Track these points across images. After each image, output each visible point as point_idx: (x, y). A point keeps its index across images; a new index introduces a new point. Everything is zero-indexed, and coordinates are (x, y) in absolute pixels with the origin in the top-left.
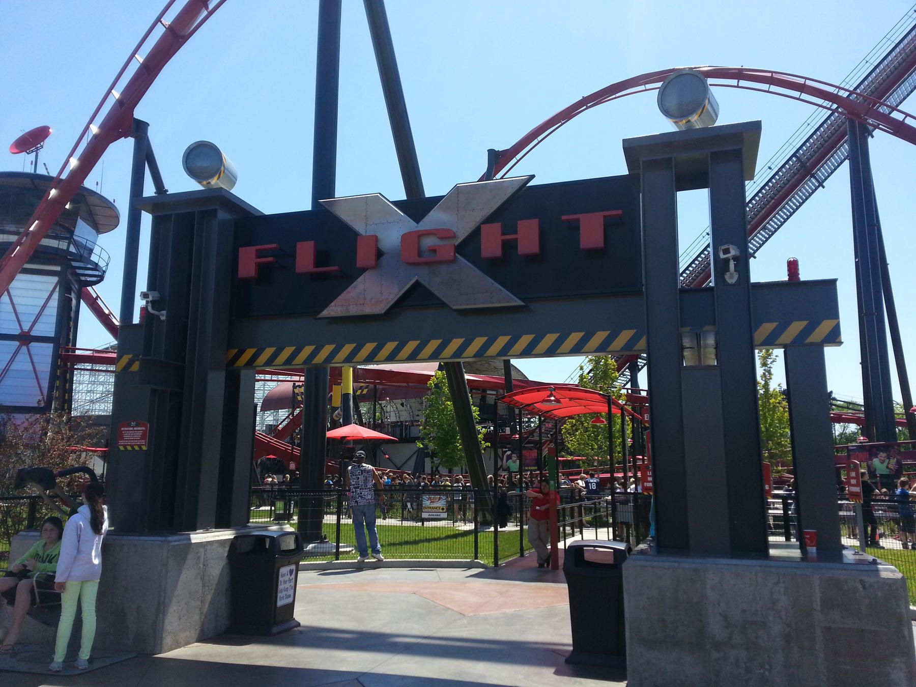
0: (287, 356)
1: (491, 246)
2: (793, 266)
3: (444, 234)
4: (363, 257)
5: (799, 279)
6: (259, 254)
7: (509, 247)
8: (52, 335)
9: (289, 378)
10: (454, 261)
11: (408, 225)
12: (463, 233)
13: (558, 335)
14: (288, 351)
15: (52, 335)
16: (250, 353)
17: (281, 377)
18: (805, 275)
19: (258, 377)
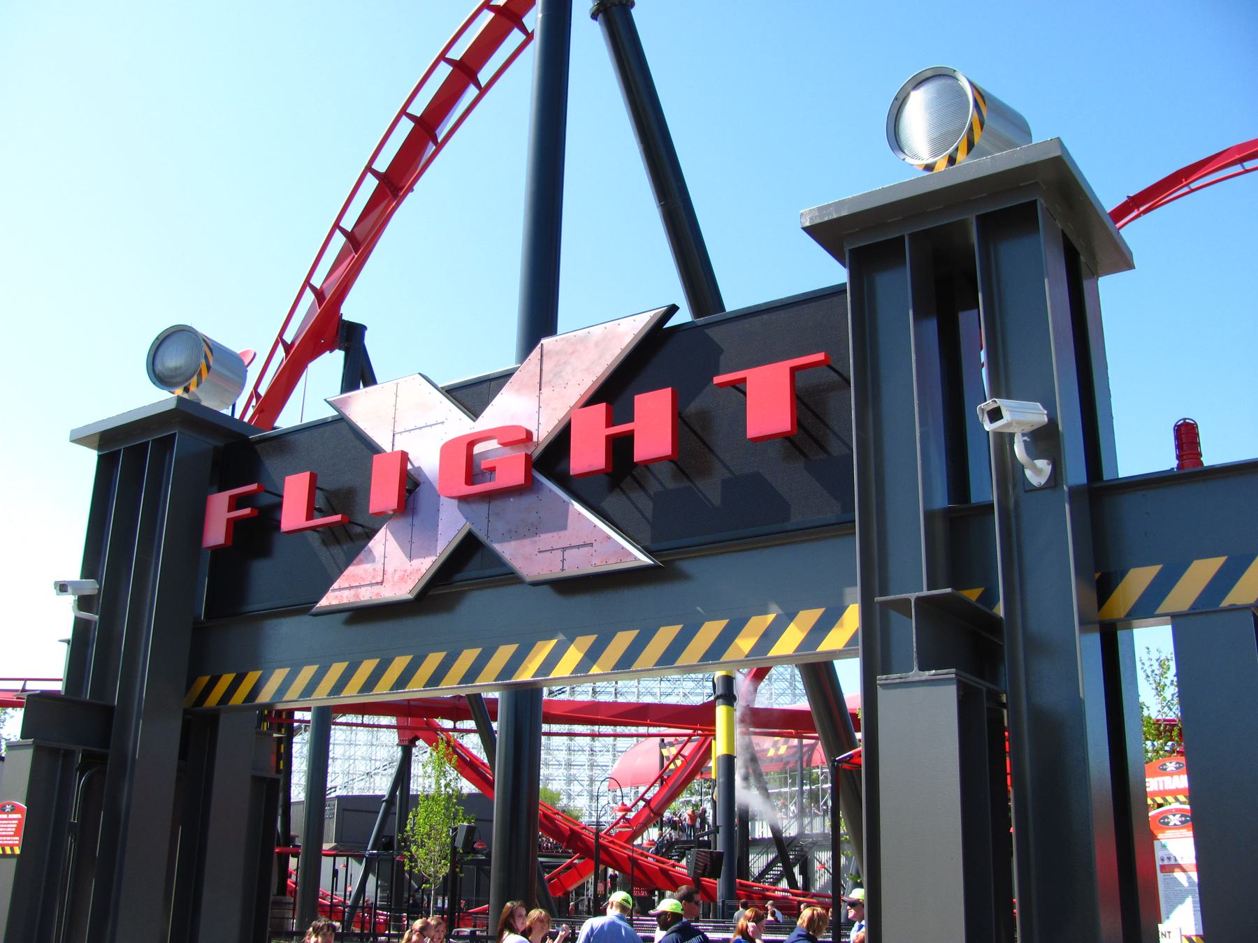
0: (280, 681)
1: (588, 456)
2: (1186, 435)
3: (519, 438)
4: (383, 495)
5: (1201, 463)
6: (235, 503)
7: (620, 447)
8: (734, 300)
9: (653, 730)
10: (529, 486)
11: (458, 424)
12: (544, 430)
13: (1224, 559)
14: (711, 631)
15: (734, 300)
16: (227, 679)
17: (620, 729)
18: (1212, 455)
19: (545, 728)
